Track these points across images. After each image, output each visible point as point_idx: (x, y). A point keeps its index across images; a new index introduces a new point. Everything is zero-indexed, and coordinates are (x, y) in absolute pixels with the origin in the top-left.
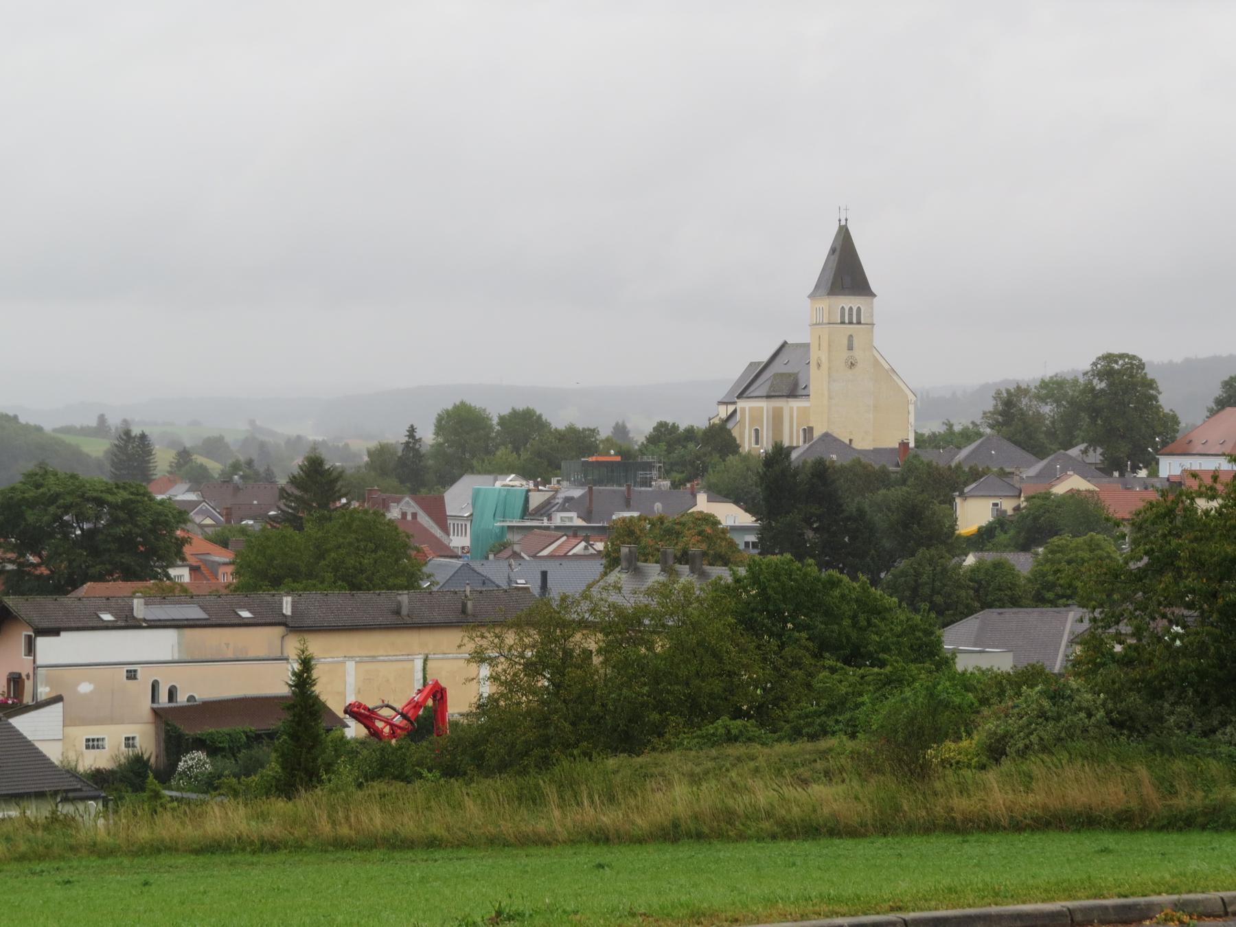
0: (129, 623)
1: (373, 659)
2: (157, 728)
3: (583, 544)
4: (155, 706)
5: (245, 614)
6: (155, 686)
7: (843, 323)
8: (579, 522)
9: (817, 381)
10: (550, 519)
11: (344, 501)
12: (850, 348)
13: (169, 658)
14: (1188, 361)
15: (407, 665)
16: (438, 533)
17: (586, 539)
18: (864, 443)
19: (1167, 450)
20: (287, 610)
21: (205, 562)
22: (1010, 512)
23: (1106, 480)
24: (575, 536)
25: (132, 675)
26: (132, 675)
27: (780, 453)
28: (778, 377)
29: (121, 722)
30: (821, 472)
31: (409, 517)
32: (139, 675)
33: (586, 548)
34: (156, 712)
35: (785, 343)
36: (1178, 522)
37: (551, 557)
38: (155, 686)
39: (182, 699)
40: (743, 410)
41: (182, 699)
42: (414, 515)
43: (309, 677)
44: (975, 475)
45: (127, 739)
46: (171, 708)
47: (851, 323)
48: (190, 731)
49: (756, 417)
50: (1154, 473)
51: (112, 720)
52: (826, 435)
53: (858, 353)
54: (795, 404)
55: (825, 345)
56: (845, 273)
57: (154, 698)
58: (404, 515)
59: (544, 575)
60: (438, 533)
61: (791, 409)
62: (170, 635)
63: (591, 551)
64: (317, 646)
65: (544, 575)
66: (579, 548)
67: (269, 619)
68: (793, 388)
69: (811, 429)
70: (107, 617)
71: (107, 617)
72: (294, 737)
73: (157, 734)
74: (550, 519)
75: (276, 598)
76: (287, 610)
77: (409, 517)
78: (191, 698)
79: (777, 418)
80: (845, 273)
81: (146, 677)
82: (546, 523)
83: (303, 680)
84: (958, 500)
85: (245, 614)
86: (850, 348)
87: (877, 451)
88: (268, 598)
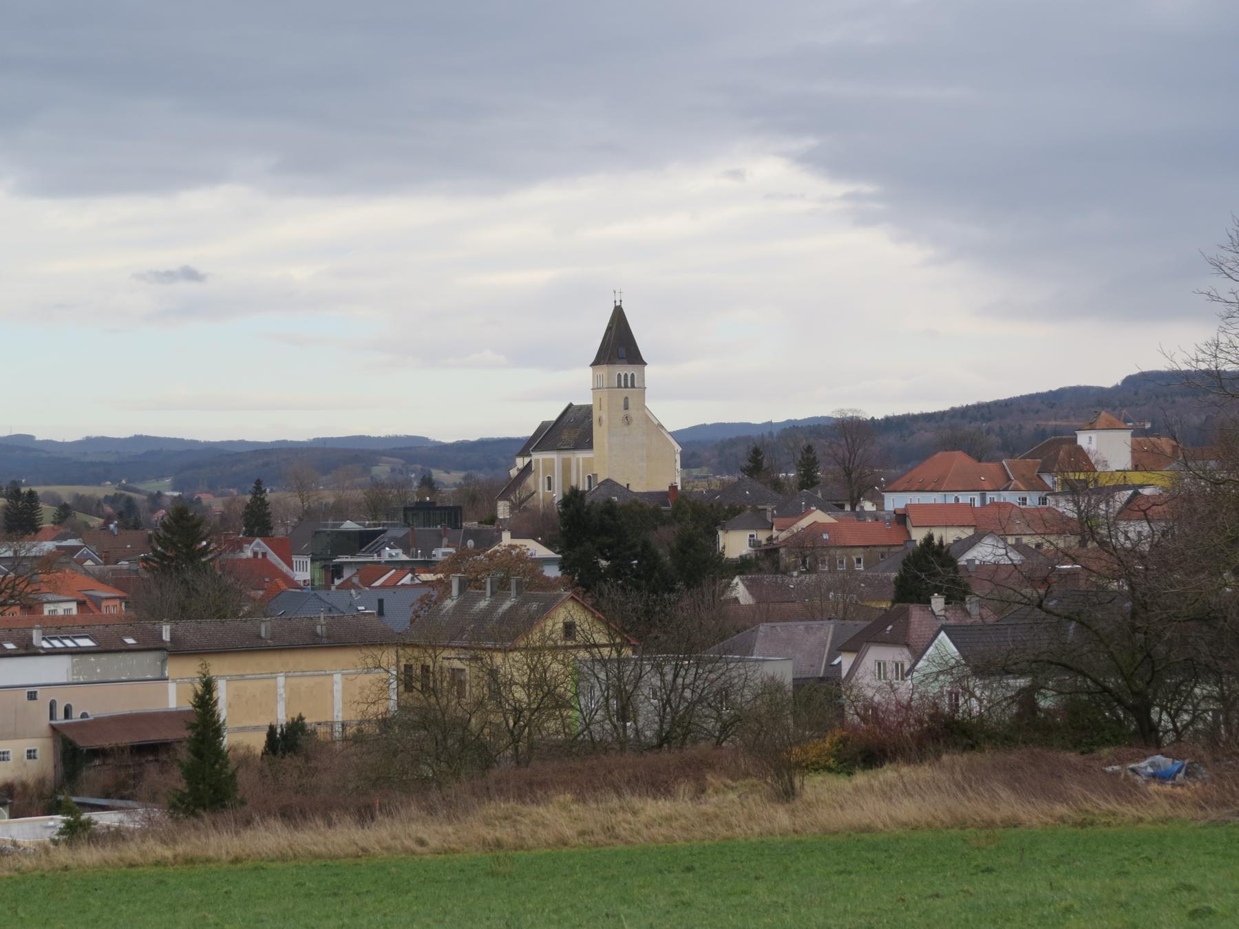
0: (28, 650)
1: (242, 677)
2: (55, 741)
3: (410, 575)
4: (53, 722)
5: (130, 641)
6: (52, 705)
7: (619, 386)
8: (404, 558)
9: (599, 434)
10: (379, 555)
11: (204, 543)
12: (626, 408)
13: (65, 680)
14: (1130, 380)
15: (271, 682)
16: (285, 568)
17: (412, 571)
18: (637, 487)
19: (891, 488)
20: (166, 636)
21: (90, 597)
22: (764, 542)
23: (841, 514)
24: (402, 569)
25: (32, 696)
26: (32, 696)
27: (573, 498)
28: (570, 430)
29: (24, 737)
30: (610, 509)
31: (260, 556)
32: (38, 696)
33: (412, 579)
34: (53, 728)
35: (571, 405)
36: (16, 593)
37: (382, 586)
38: (52, 705)
39: (76, 716)
40: (537, 461)
41: (76, 716)
42: (264, 554)
43: (211, 699)
44: (734, 512)
45: (29, 751)
46: (67, 724)
47: (626, 386)
48: (84, 744)
49: (549, 466)
50: (880, 504)
51: (15, 736)
52: (608, 480)
53: (632, 412)
54: (581, 456)
55: (605, 407)
56: (619, 346)
57: (52, 717)
58: (255, 554)
59: (381, 602)
60: (285, 568)
61: (578, 459)
62: (65, 662)
63: (417, 581)
64: (219, 667)
65: (381, 602)
66: (407, 579)
67: (150, 645)
68: (584, 441)
69: (595, 475)
70: (10, 646)
71: (10, 646)
72: (198, 753)
73: (55, 746)
74: (379, 555)
75: (157, 626)
76: (166, 636)
77: (260, 556)
78: (84, 715)
79: (566, 468)
80: (619, 346)
81: (44, 697)
82: (376, 558)
83: (205, 700)
84: (720, 533)
85: (130, 641)
86: (626, 408)
87: (650, 495)
88: (149, 626)
